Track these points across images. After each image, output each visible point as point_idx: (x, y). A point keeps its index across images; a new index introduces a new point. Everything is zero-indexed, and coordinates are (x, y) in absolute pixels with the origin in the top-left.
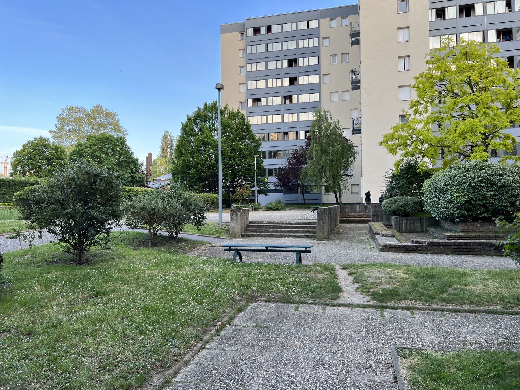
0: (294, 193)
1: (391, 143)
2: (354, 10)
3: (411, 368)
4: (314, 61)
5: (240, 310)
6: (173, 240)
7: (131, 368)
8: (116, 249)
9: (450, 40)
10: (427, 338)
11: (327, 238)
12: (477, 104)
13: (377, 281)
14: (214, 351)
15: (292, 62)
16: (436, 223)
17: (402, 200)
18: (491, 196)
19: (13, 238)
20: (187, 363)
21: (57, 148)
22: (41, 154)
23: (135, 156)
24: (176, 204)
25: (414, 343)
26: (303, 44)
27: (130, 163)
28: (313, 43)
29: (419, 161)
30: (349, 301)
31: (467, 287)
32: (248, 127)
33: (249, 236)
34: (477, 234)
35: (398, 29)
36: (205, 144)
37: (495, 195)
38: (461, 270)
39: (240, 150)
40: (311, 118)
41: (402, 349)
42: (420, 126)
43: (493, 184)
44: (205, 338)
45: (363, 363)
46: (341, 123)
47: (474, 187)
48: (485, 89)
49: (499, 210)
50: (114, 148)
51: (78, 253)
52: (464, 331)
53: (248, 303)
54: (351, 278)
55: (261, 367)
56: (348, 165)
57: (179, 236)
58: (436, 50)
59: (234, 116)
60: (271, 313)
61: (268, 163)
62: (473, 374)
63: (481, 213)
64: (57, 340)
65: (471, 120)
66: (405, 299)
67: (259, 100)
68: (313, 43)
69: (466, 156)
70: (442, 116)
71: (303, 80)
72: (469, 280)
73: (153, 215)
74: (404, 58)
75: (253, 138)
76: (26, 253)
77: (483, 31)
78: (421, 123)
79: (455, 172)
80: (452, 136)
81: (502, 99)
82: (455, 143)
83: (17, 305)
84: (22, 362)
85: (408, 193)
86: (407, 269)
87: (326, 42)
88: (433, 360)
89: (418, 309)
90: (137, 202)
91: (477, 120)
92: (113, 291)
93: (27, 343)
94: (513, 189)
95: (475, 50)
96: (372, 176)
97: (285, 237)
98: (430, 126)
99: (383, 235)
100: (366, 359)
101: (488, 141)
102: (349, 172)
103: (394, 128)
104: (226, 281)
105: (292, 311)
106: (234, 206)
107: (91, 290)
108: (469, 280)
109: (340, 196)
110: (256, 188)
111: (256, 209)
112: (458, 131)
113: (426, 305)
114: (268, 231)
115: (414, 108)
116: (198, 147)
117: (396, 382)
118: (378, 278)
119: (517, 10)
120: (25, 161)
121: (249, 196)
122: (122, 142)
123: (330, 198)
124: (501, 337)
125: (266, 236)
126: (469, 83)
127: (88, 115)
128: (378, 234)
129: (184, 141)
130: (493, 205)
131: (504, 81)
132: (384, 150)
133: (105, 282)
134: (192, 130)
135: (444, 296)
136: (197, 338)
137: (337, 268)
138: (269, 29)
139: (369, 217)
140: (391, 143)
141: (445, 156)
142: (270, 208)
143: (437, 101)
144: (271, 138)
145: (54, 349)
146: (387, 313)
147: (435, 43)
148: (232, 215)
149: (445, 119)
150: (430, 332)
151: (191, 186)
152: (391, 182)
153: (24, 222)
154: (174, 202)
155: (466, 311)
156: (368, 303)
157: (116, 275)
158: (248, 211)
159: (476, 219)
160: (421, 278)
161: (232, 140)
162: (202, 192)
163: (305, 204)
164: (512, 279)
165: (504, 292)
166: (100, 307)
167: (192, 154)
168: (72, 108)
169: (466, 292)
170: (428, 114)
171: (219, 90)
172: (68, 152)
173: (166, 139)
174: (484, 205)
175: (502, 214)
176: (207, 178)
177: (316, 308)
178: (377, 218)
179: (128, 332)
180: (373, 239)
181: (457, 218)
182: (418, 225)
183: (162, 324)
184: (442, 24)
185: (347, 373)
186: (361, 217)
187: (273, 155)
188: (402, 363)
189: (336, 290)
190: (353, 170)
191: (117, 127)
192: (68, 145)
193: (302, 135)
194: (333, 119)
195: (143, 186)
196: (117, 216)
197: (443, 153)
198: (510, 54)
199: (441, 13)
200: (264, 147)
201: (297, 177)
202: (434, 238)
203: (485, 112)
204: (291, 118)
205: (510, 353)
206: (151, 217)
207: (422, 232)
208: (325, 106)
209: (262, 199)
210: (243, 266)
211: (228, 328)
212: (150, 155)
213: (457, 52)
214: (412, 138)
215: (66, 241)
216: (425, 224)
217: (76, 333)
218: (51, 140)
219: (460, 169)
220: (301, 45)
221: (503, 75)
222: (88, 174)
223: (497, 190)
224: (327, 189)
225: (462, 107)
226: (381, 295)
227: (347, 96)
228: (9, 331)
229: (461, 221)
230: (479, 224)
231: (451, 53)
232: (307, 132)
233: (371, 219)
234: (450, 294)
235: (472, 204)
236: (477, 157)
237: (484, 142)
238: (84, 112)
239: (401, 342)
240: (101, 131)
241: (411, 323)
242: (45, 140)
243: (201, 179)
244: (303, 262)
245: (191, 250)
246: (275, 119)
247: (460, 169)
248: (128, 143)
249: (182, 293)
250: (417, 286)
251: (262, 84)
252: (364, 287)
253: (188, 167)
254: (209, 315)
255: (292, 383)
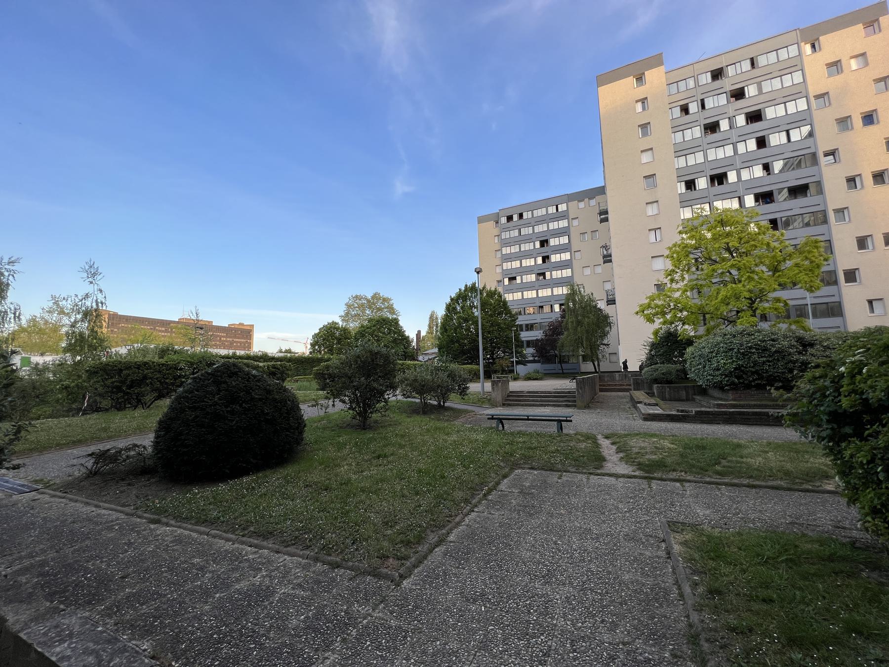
0: (552, 363)
1: (647, 312)
2: (601, 191)
3: (685, 543)
4: (564, 240)
5: (505, 477)
6: (440, 408)
7: (410, 526)
8: (394, 416)
9: (702, 209)
10: (701, 512)
11: (587, 407)
12: (739, 269)
13: (643, 451)
14: (482, 515)
15: (544, 243)
16: (703, 392)
17: (663, 368)
18: (764, 362)
19: (313, 406)
20: (458, 524)
21: (345, 330)
22: (333, 335)
23: (407, 334)
24: (443, 376)
25: (686, 517)
26: (554, 226)
27: (402, 340)
28: (563, 224)
29: (679, 328)
30: (613, 471)
31: (744, 460)
32: (505, 303)
33: (509, 405)
34: (750, 403)
35: (642, 152)
36: (466, 320)
37: (769, 361)
38: (735, 441)
39: (498, 325)
40: (565, 292)
41: (674, 523)
42: (677, 295)
43: (765, 349)
44: (474, 501)
45: (632, 536)
46: (595, 296)
47: (743, 353)
48: (747, 254)
49: (775, 377)
50: (386, 327)
51: (363, 419)
52: (744, 507)
53: (512, 470)
54: (614, 447)
55: (527, 533)
56: (605, 335)
57: (447, 404)
58: (688, 220)
59: (491, 294)
60: (535, 480)
61: (525, 336)
62: (758, 555)
63: (754, 380)
64: (348, 496)
65: (734, 285)
66: (674, 470)
67: (515, 278)
68: (563, 224)
69: (731, 322)
70: (700, 282)
71: (555, 258)
72: (746, 452)
73: (423, 386)
74: (655, 230)
75: (510, 313)
76: (322, 419)
77: (739, 198)
78: (678, 291)
79: (720, 339)
80: (713, 303)
81: (767, 262)
82: (717, 309)
83: (316, 463)
84: (321, 514)
85: (670, 361)
86: (674, 439)
87: (575, 223)
88: (710, 537)
89: (689, 481)
90: (409, 374)
91: (740, 285)
92: (392, 454)
93: (325, 496)
94: (789, 354)
95: (732, 217)
96: (631, 343)
97: (545, 406)
98: (688, 293)
99: (645, 404)
100: (635, 532)
101: (755, 305)
102: (605, 342)
103: (649, 297)
104: (490, 448)
105: (556, 479)
106: (494, 377)
107: (374, 453)
108: (746, 452)
109: (599, 365)
110: (515, 359)
111: (515, 379)
112: (720, 297)
113: (698, 478)
114: (528, 401)
115: (669, 277)
116: (460, 324)
117: (669, 558)
118: (643, 448)
119: (776, 171)
120: (321, 341)
121: (508, 367)
122: (396, 321)
123: (588, 367)
124: (790, 516)
125: (526, 405)
126: (728, 249)
127: (368, 301)
128: (640, 402)
129: (447, 318)
130: (767, 371)
131: (768, 244)
132: (641, 319)
133: (385, 446)
134: (455, 309)
135: (718, 468)
136: (467, 501)
137: (599, 437)
138: (521, 216)
139: (630, 385)
140: (647, 312)
141: (707, 322)
142: (528, 378)
143: (694, 269)
144: (527, 312)
145: (346, 504)
146: (655, 484)
147: (687, 214)
148: (493, 385)
149: (704, 286)
150: (702, 506)
151: (455, 359)
152: (651, 351)
153: (321, 392)
154: (440, 374)
155: (745, 486)
156: (633, 474)
157: (394, 440)
158: (508, 381)
159: (748, 387)
160: (691, 448)
161: (491, 316)
162: (464, 364)
163: (563, 373)
164: (797, 452)
165: (789, 466)
166: (382, 468)
167: (455, 329)
168: (357, 297)
169: (743, 465)
170: (685, 282)
171: (478, 273)
172: (353, 333)
173: (432, 318)
174: (756, 372)
175: (780, 381)
176: (469, 351)
177: (580, 476)
178: (638, 386)
179: (405, 492)
180: (636, 408)
181: (727, 385)
182: (683, 394)
183: (434, 487)
184: (692, 194)
185: (615, 545)
186: (621, 385)
187: (530, 327)
188: (675, 538)
189: (599, 460)
190: (610, 339)
191: (391, 309)
192: (353, 326)
193: (557, 308)
194: (587, 291)
195: (414, 359)
196: (393, 387)
197: (705, 320)
198: (772, 217)
199: (690, 185)
200: (521, 320)
201: (554, 347)
202: (702, 406)
203: (749, 277)
204: (545, 293)
205: (804, 535)
206: (421, 388)
207: (687, 400)
208: (577, 280)
209: (521, 369)
210: (505, 434)
211: (494, 492)
212: (419, 332)
213: (712, 220)
214: (670, 306)
215: (353, 409)
216: (691, 392)
217: (363, 490)
218: (341, 323)
219: (725, 335)
220: (551, 227)
221: (766, 238)
222: (371, 352)
223: (770, 356)
224: (585, 358)
225: (722, 273)
226: (647, 466)
227: (599, 270)
228: (311, 486)
229: (732, 389)
230: (753, 392)
231: (705, 221)
232: (561, 305)
233: (632, 387)
234: (724, 467)
235: (742, 371)
236: (744, 323)
237: (751, 307)
238: (366, 299)
239: (672, 515)
240: (379, 314)
241: (683, 496)
242: (336, 323)
243: (463, 352)
244: (565, 431)
245: (457, 418)
246: (530, 294)
247: (725, 335)
248: (401, 323)
249: (451, 458)
250: (686, 457)
251: (516, 264)
252: (628, 458)
253: (452, 342)
254: (477, 480)
255: (560, 551)
